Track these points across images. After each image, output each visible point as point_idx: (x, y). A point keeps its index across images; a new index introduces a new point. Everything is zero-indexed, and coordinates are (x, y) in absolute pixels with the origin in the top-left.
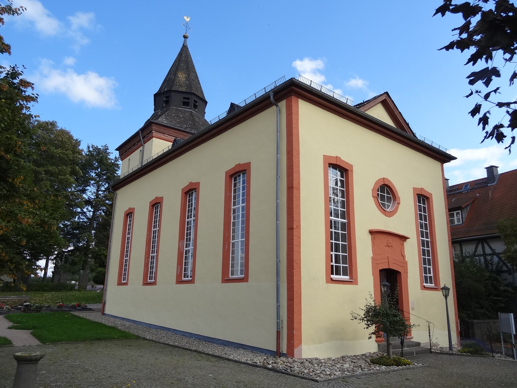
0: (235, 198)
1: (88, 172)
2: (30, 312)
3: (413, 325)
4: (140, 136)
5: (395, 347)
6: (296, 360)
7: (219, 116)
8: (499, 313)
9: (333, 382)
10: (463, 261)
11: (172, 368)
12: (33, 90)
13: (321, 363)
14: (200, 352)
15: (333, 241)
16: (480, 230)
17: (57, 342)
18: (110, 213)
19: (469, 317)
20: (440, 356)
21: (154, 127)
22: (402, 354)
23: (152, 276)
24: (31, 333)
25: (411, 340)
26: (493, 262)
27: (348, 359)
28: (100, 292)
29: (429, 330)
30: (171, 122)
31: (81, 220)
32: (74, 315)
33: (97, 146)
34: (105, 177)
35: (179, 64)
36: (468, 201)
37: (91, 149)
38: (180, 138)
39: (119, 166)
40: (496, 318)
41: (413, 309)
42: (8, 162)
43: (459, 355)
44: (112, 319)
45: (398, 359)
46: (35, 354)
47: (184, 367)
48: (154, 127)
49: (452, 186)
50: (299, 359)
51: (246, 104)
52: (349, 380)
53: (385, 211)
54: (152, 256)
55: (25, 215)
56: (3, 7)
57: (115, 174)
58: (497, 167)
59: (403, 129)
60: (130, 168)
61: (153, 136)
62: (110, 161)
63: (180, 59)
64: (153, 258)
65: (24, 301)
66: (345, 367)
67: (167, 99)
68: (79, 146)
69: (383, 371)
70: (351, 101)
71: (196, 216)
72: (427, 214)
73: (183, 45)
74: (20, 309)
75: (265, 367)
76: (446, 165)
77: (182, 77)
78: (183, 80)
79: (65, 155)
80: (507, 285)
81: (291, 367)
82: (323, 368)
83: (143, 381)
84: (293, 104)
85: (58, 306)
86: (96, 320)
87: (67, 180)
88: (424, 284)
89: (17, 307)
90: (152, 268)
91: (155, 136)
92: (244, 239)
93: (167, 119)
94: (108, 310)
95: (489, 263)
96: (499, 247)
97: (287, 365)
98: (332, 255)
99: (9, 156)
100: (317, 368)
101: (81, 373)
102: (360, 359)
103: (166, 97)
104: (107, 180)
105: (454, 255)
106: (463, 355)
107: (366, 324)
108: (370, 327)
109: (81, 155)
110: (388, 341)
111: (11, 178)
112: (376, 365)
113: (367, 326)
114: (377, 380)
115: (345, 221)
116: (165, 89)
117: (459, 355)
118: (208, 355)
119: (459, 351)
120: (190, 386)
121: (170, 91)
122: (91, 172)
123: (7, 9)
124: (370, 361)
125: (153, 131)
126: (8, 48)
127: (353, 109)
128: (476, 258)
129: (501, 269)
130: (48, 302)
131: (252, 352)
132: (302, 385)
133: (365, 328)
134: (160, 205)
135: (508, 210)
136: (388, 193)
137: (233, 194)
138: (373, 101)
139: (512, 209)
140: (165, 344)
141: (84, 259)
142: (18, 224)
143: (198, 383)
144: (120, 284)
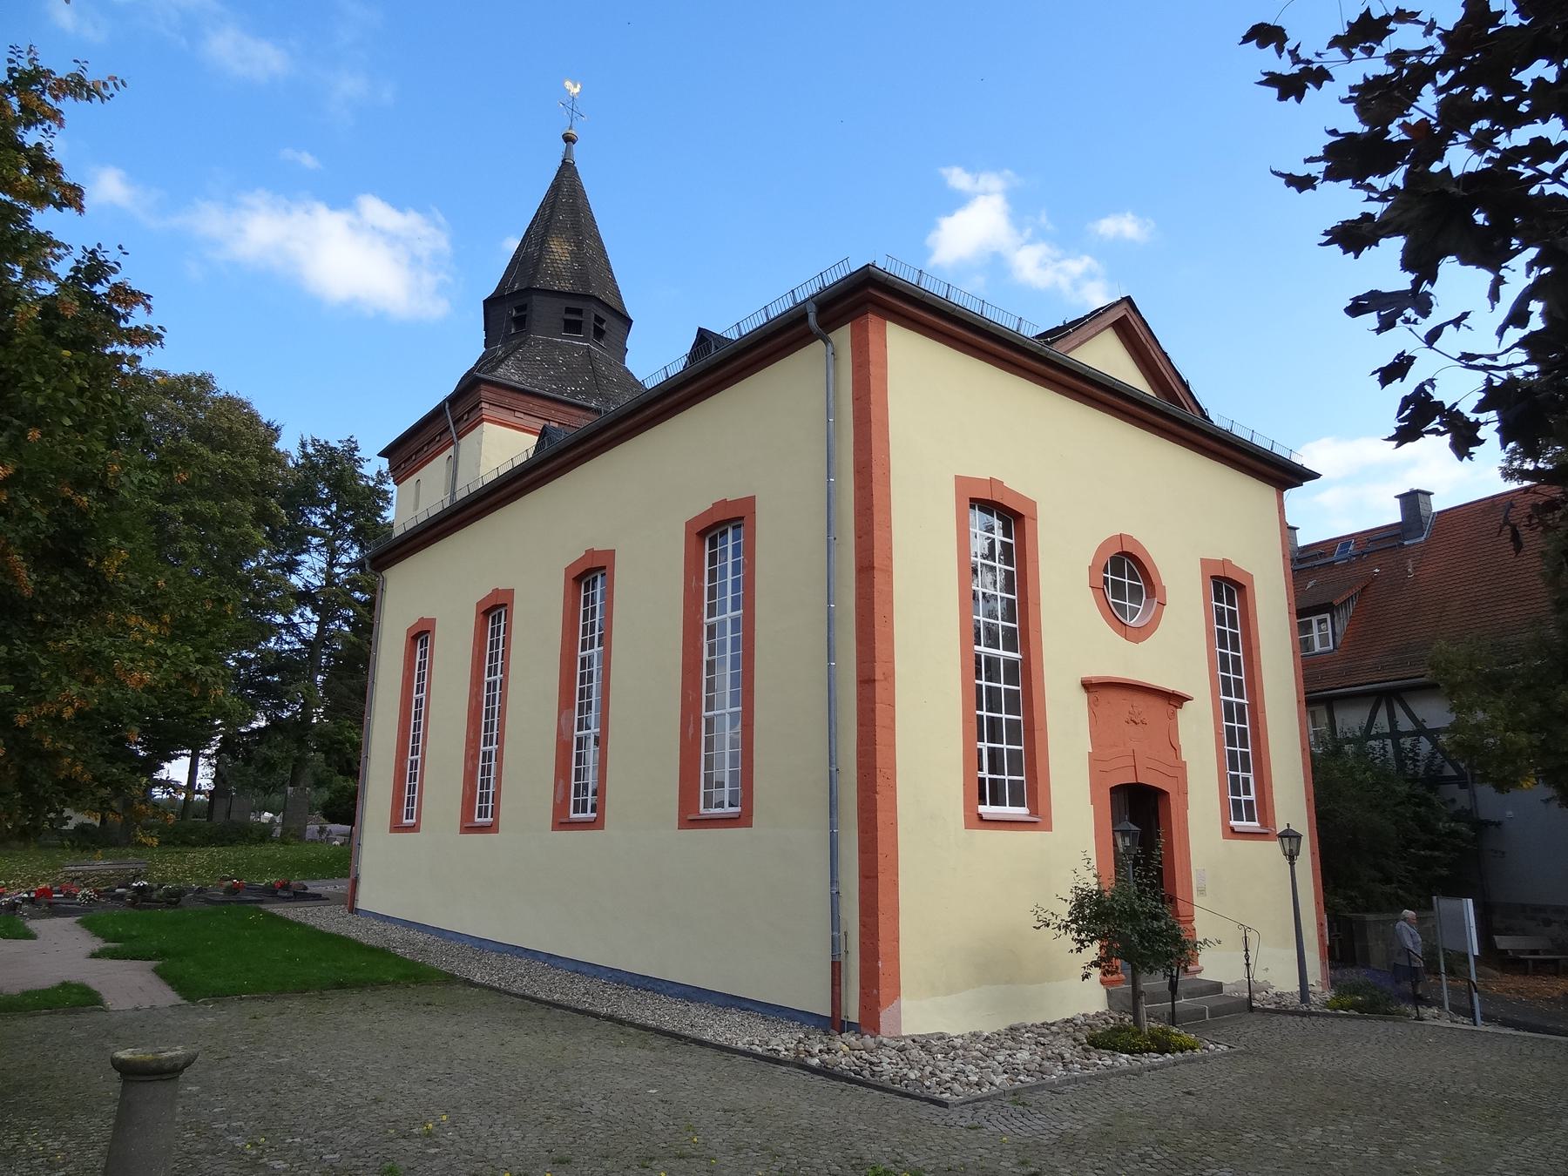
0: (712, 595)
1: (304, 514)
2: (149, 907)
3: (1202, 941)
4: (447, 417)
5: (1155, 998)
6: (885, 1041)
7: (668, 368)
8: (1435, 898)
9: (989, 1105)
10: (1336, 752)
11: (546, 1071)
12: (149, 312)
13: (954, 1048)
14: (621, 1022)
15: (985, 713)
16: (1382, 667)
17: (227, 996)
18: (366, 627)
19: (1353, 905)
20: (1275, 1019)
21: (485, 392)
22: (1173, 1019)
23: (487, 808)
24: (156, 970)
25: (1198, 976)
26: (1417, 755)
27: (1026, 1035)
28: (342, 845)
29: (1247, 950)
31: (286, 647)
32: (273, 915)
33: (326, 443)
34: (351, 527)
35: (552, 212)
36: (1351, 588)
37: (310, 450)
38: (559, 423)
39: (390, 496)
40: (1425, 908)
41: (1202, 892)
42: (82, 514)
43: (1326, 1015)
44: (378, 926)
45: (1163, 1033)
46: (170, 1054)
47: (579, 1066)
48: (485, 392)
49: (1304, 547)
50: (893, 1038)
51: (740, 334)
52: (1031, 1099)
53: (1125, 625)
54: (484, 753)
55: (132, 660)
56: (61, 79)
57: (378, 519)
58: (1429, 494)
59: (1173, 398)
60: (422, 507)
61: (484, 416)
62: (363, 483)
63: (554, 202)
64: (487, 756)
65: (131, 874)
66: (1018, 1062)
67: (519, 314)
68: (276, 439)
69: (1121, 1068)
70: (1032, 324)
71: (605, 640)
72: (1239, 632)
73: (563, 161)
74: (121, 897)
75: (801, 1065)
76: (1290, 494)
78: (563, 258)
79: (239, 468)
80: (1456, 817)
81: (871, 1063)
82: (958, 1064)
83: (468, 1111)
84: (871, 336)
85: (228, 887)
86: (334, 930)
87: (247, 537)
88: (1233, 823)
89: (114, 891)
90: (485, 784)
91: (487, 417)
92: (740, 708)
93: (520, 368)
94: (367, 899)
95: (1406, 756)
96: (1435, 713)
97: (861, 1057)
98: (980, 751)
99: (85, 499)
100: (942, 1065)
101: (297, 1090)
102: (1058, 1034)
103: (518, 309)
104: (358, 536)
105: (1312, 738)
106: (1338, 1016)
107: (1076, 939)
108: (1085, 947)
109: (283, 466)
110: (1135, 983)
111: (92, 558)
112: (1103, 1051)
113: (1079, 945)
114: (1107, 1097)
115: (1017, 656)
116: (513, 284)
117: (1326, 1015)
118: (645, 1028)
119: (1327, 1005)
120: (598, 1125)
121: (528, 291)
122: (311, 512)
123: (73, 84)
124: (1085, 1041)
125: (483, 405)
126: (77, 195)
127: (1037, 347)
128: (1372, 743)
129: (1440, 772)
130: (198, 876)
131: (763, 1017)
132: (904, 1118)
133: (1072, 951)
134: (506, 611)
135: (1459, 611)
136: (1133, 576)
137: (706, 585)
138: (1090, 325)
139: (1470, 609)
140: (524, 997)
141: (296, 753)
142: (115, 690)
143: (621, 1117)
144: (397, 827)
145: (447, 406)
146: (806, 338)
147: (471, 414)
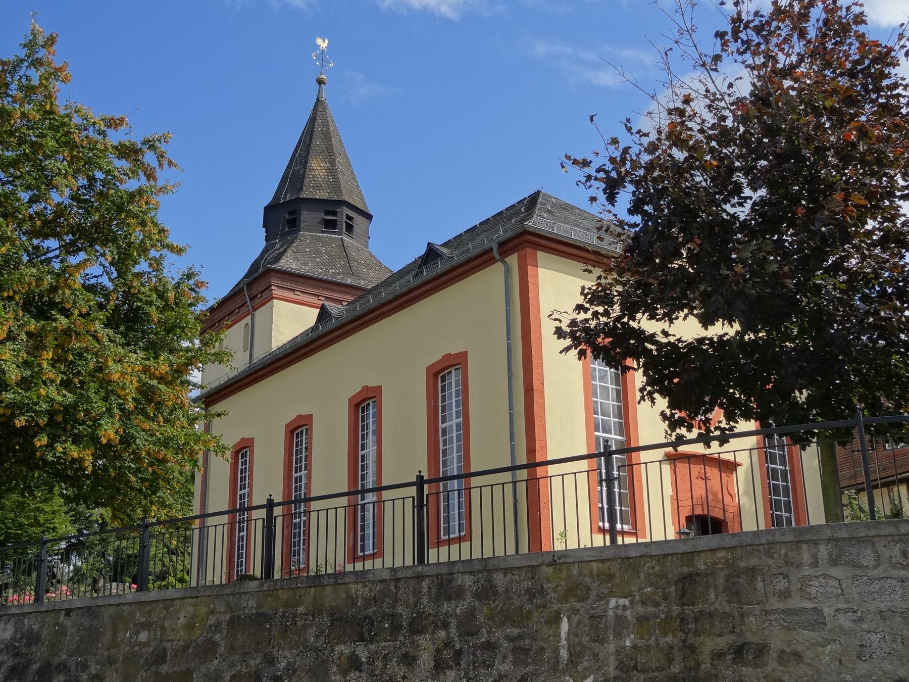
30: (306, 264)
73: (318, 99)
77: (319, 168)
78: (321, 174)
93: (296, 258)
103: (290, 213)
145: (245, 288)
146: (492, 261)
147: (263, 294)
